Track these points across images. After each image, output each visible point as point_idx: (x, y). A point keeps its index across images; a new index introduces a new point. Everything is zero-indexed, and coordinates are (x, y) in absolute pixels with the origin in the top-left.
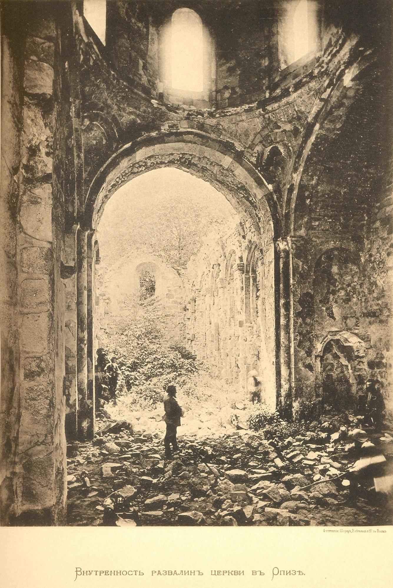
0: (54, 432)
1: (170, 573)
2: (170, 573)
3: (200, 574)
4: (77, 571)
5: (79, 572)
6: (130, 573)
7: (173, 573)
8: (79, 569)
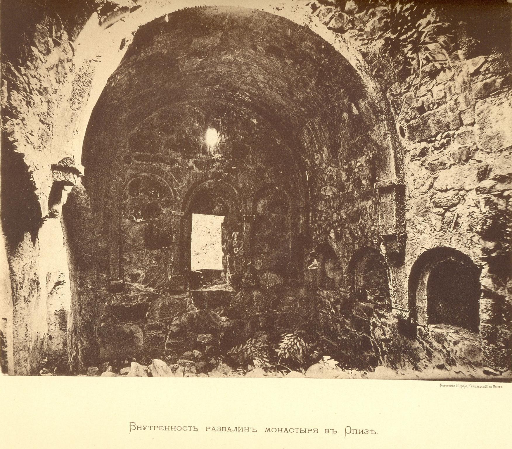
0: (452, 371)
1: (223, 429)
2: (223, 429)
3: (334, 432)
4: (131, 426)
5: (133, 426)
6: (291, 430)
7: (227, 429)
8: (134, 424)
